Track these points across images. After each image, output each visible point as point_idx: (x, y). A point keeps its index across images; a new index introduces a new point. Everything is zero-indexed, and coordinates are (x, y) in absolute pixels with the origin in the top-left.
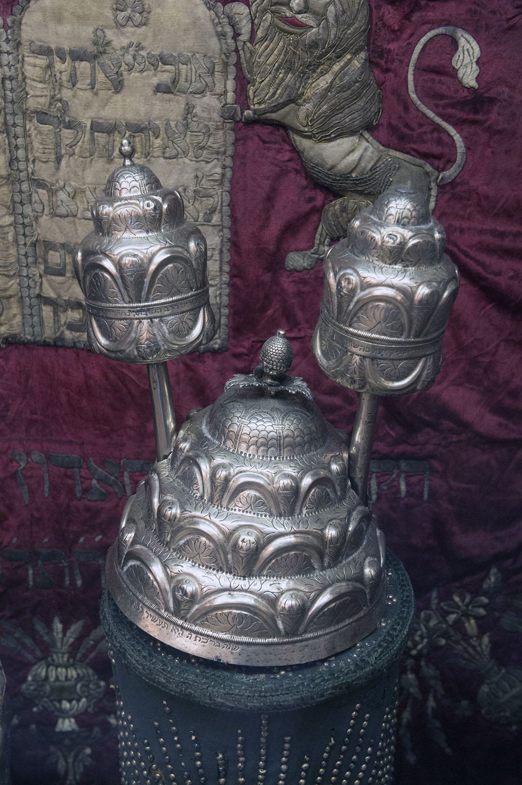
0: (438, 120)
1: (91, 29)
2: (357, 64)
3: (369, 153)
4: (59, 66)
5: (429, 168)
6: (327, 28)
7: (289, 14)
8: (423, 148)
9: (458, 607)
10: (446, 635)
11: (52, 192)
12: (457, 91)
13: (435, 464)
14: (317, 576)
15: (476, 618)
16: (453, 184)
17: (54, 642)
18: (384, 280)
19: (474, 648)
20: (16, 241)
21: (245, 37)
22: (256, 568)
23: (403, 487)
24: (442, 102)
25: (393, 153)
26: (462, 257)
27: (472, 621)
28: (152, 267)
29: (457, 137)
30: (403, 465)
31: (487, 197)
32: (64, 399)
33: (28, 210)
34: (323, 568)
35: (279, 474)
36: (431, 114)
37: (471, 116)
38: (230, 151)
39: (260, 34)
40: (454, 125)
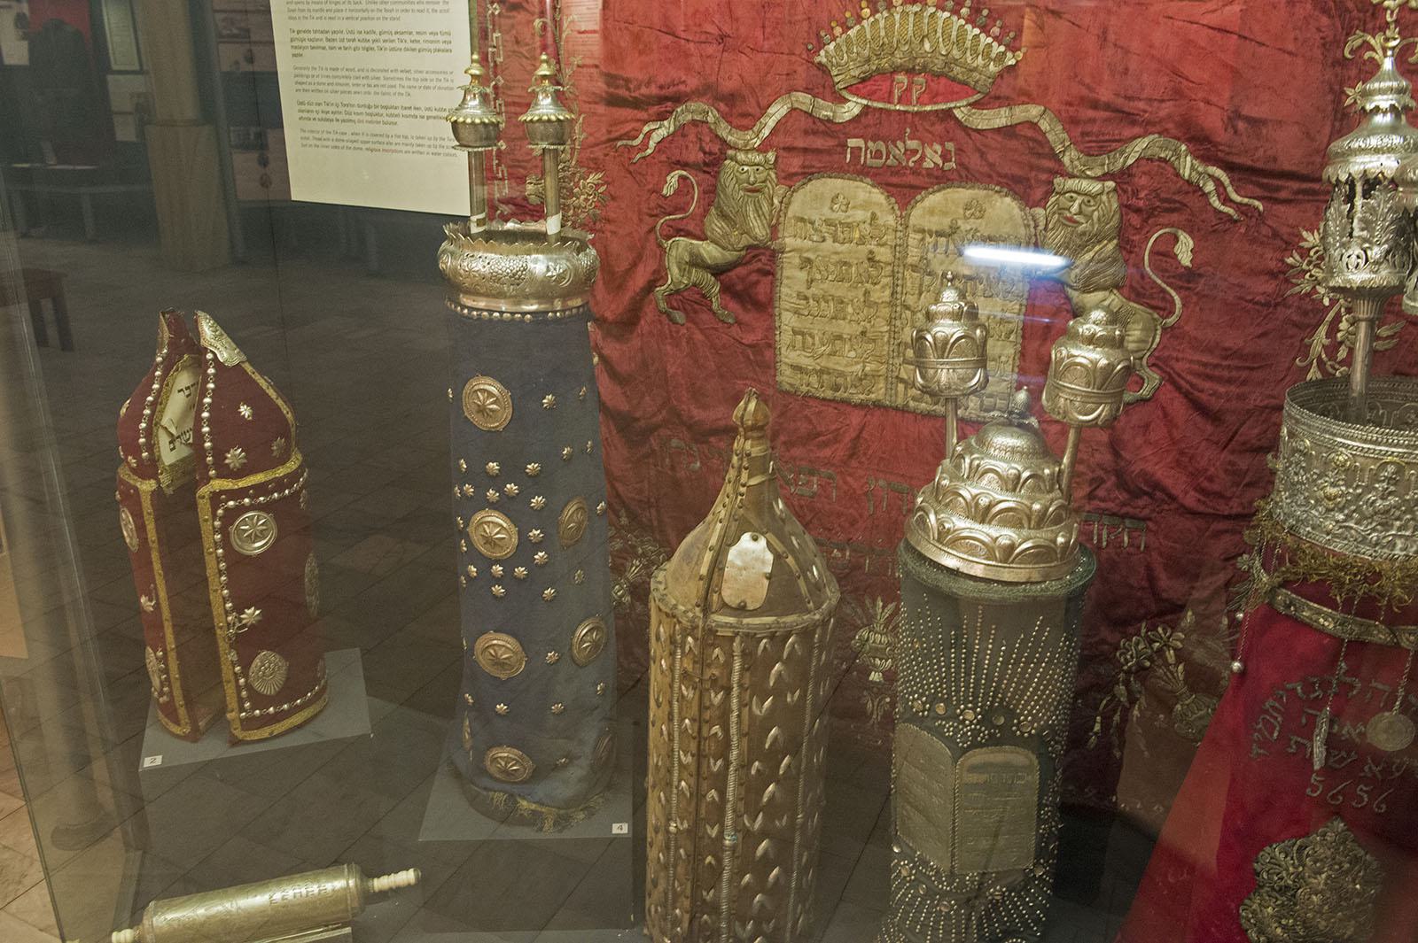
0: (1164, 286)
1: (949, 220)
2: (1111, 246)
3: (1115, 302)
4: (928, 239)
5: (1156, 316)
6: (1092, 225)
7: (1068, 215)
8: (1153, 303)
9: (1161, 638)
10: (1150, 659)
11: (914, 313)
12: (1177, 268)
13: (1151, 524)
14: (1025, 532)
15: (1175, 649)
16: (1172, 327)
17: (876, 614)
18: (1087, 355)
19: (1172, 673)
20: (889, 341)
21: (1041, 227)
22: (988, 519)
23: (1126, 539)
24: (1167, 274)
25: (1132, 304)
26: (1176, 378)
27: (1172, 652)
28: (952, 341)
29: (1177, 298)
30: (1127, 522)
31: (1196, 338)
32: (903, 446)
33: (898, 323)
34: (1029, 528)
35: (1008, 468)
36: (1159, 282)
37: (1186, 285)
38: (1026, 296)
39: (1050, 226)
40: (1175, 289)
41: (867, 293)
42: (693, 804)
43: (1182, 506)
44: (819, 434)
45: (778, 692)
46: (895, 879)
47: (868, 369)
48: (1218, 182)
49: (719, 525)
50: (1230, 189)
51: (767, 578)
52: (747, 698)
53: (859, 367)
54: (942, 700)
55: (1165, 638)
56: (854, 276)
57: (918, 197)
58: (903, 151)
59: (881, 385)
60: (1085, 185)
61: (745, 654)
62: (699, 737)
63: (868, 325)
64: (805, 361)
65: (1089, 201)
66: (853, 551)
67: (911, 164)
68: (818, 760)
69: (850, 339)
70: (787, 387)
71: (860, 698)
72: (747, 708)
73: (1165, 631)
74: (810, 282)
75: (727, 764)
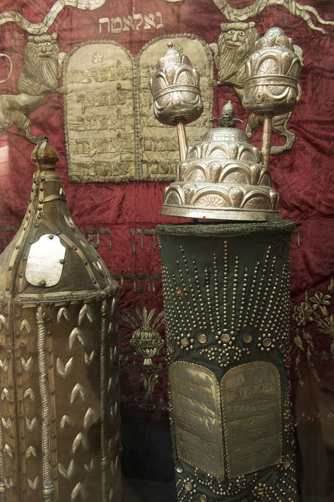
7: (232, 43)
9: (318, 301)
15: (326, 306)
17: (143, 319)
20: (135, 139)
27: (325, 308)
33: (139, 126)
41: (119, 110)
42: (16, 463)
43: (319, 212)
44: (97, 206)
45: (77, 354)
46: (181, 496)
47: (123, 157)
48: (310, 13)
49: (24, 232)
50: (318, 17)
51: (61, 263)
52: (52, 361)
53: (118, 158)
54: (203, 331)
55: (320, 300)
56: (110, 101)
57: (144, 47)
58: (132, 21)
59: (132, 168)
60: (238, 25)
61: (47, 322)
62: (16, 403)
63: (121, 131)
64: (85, 160)
65: (242, 33)
66: (125, 279)
67: (138, 29)
68: (114, 412)
69: (111, 141)
70: (75, 178)
71: (139, 379)
72: (53, 369)
73: (319, 295)
74: (84, 110)
75: (40, 421)
